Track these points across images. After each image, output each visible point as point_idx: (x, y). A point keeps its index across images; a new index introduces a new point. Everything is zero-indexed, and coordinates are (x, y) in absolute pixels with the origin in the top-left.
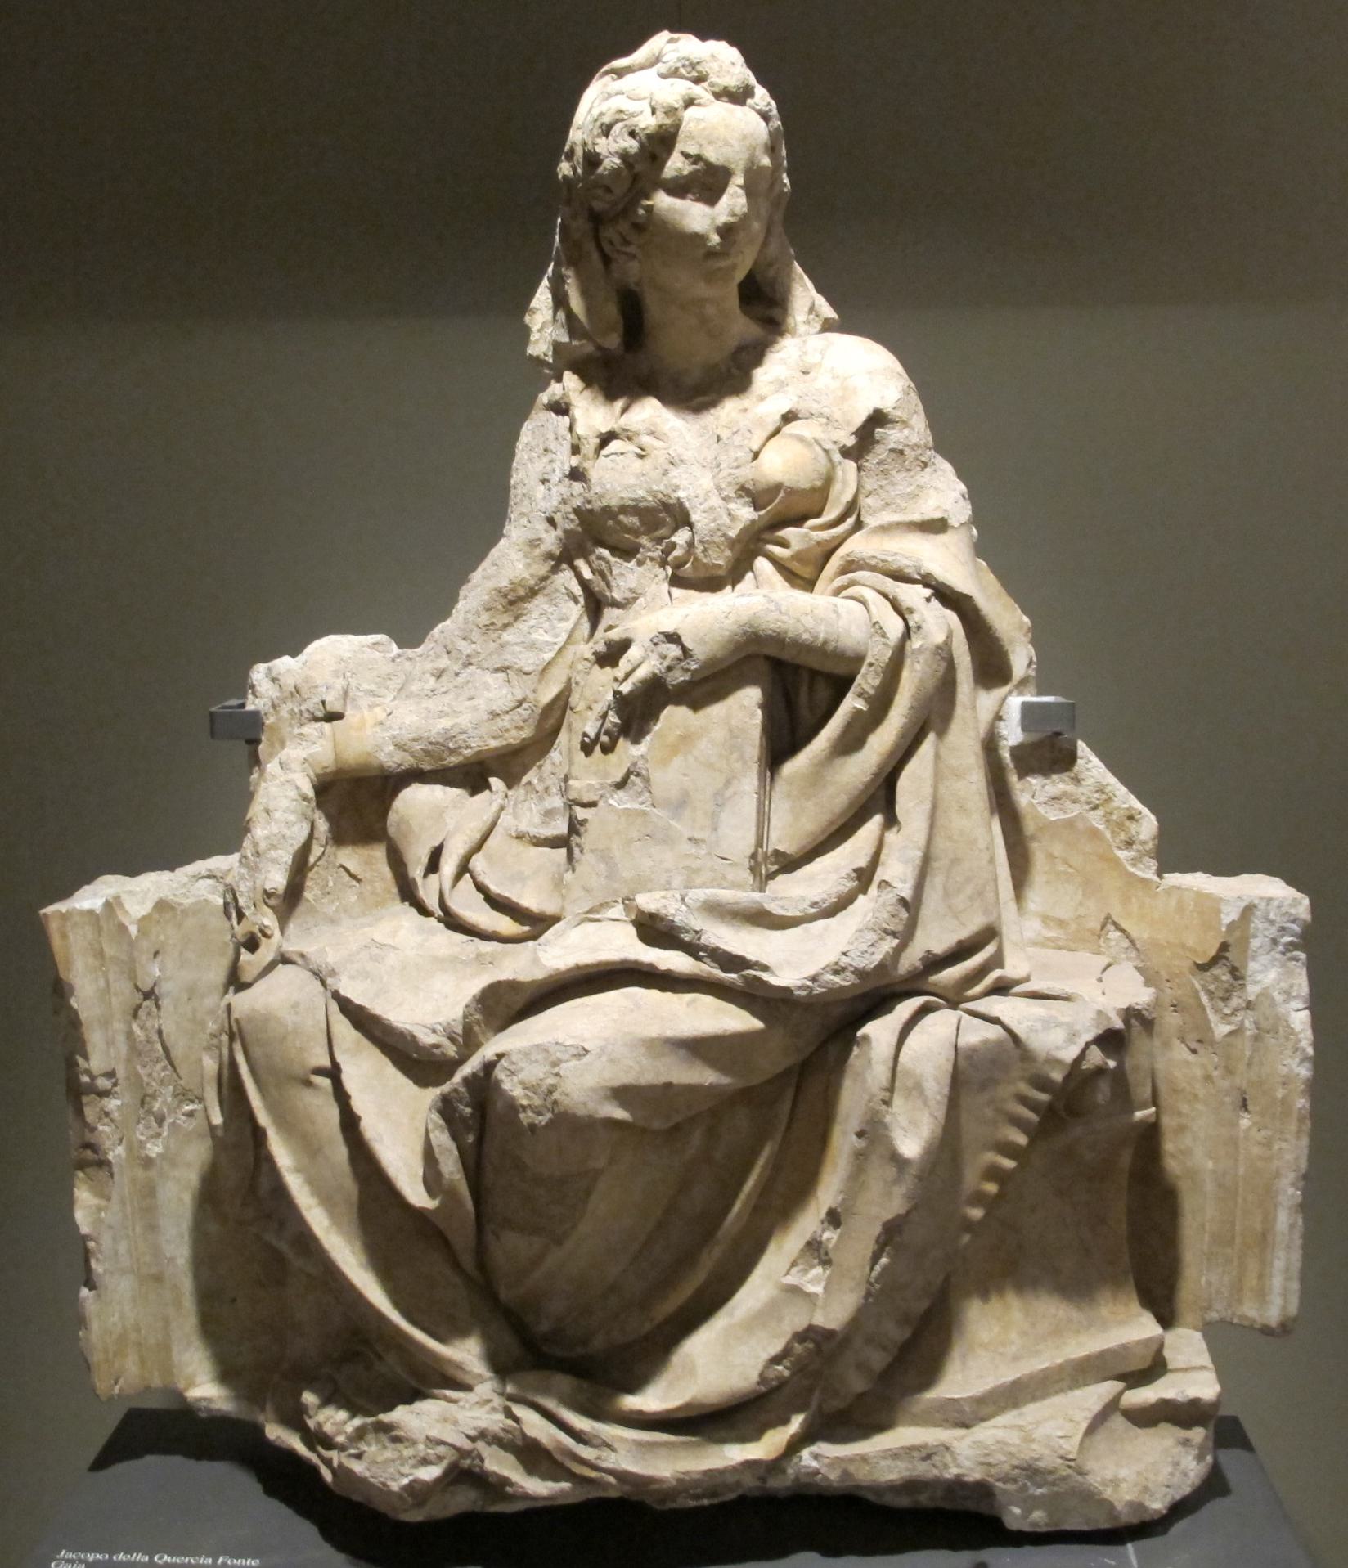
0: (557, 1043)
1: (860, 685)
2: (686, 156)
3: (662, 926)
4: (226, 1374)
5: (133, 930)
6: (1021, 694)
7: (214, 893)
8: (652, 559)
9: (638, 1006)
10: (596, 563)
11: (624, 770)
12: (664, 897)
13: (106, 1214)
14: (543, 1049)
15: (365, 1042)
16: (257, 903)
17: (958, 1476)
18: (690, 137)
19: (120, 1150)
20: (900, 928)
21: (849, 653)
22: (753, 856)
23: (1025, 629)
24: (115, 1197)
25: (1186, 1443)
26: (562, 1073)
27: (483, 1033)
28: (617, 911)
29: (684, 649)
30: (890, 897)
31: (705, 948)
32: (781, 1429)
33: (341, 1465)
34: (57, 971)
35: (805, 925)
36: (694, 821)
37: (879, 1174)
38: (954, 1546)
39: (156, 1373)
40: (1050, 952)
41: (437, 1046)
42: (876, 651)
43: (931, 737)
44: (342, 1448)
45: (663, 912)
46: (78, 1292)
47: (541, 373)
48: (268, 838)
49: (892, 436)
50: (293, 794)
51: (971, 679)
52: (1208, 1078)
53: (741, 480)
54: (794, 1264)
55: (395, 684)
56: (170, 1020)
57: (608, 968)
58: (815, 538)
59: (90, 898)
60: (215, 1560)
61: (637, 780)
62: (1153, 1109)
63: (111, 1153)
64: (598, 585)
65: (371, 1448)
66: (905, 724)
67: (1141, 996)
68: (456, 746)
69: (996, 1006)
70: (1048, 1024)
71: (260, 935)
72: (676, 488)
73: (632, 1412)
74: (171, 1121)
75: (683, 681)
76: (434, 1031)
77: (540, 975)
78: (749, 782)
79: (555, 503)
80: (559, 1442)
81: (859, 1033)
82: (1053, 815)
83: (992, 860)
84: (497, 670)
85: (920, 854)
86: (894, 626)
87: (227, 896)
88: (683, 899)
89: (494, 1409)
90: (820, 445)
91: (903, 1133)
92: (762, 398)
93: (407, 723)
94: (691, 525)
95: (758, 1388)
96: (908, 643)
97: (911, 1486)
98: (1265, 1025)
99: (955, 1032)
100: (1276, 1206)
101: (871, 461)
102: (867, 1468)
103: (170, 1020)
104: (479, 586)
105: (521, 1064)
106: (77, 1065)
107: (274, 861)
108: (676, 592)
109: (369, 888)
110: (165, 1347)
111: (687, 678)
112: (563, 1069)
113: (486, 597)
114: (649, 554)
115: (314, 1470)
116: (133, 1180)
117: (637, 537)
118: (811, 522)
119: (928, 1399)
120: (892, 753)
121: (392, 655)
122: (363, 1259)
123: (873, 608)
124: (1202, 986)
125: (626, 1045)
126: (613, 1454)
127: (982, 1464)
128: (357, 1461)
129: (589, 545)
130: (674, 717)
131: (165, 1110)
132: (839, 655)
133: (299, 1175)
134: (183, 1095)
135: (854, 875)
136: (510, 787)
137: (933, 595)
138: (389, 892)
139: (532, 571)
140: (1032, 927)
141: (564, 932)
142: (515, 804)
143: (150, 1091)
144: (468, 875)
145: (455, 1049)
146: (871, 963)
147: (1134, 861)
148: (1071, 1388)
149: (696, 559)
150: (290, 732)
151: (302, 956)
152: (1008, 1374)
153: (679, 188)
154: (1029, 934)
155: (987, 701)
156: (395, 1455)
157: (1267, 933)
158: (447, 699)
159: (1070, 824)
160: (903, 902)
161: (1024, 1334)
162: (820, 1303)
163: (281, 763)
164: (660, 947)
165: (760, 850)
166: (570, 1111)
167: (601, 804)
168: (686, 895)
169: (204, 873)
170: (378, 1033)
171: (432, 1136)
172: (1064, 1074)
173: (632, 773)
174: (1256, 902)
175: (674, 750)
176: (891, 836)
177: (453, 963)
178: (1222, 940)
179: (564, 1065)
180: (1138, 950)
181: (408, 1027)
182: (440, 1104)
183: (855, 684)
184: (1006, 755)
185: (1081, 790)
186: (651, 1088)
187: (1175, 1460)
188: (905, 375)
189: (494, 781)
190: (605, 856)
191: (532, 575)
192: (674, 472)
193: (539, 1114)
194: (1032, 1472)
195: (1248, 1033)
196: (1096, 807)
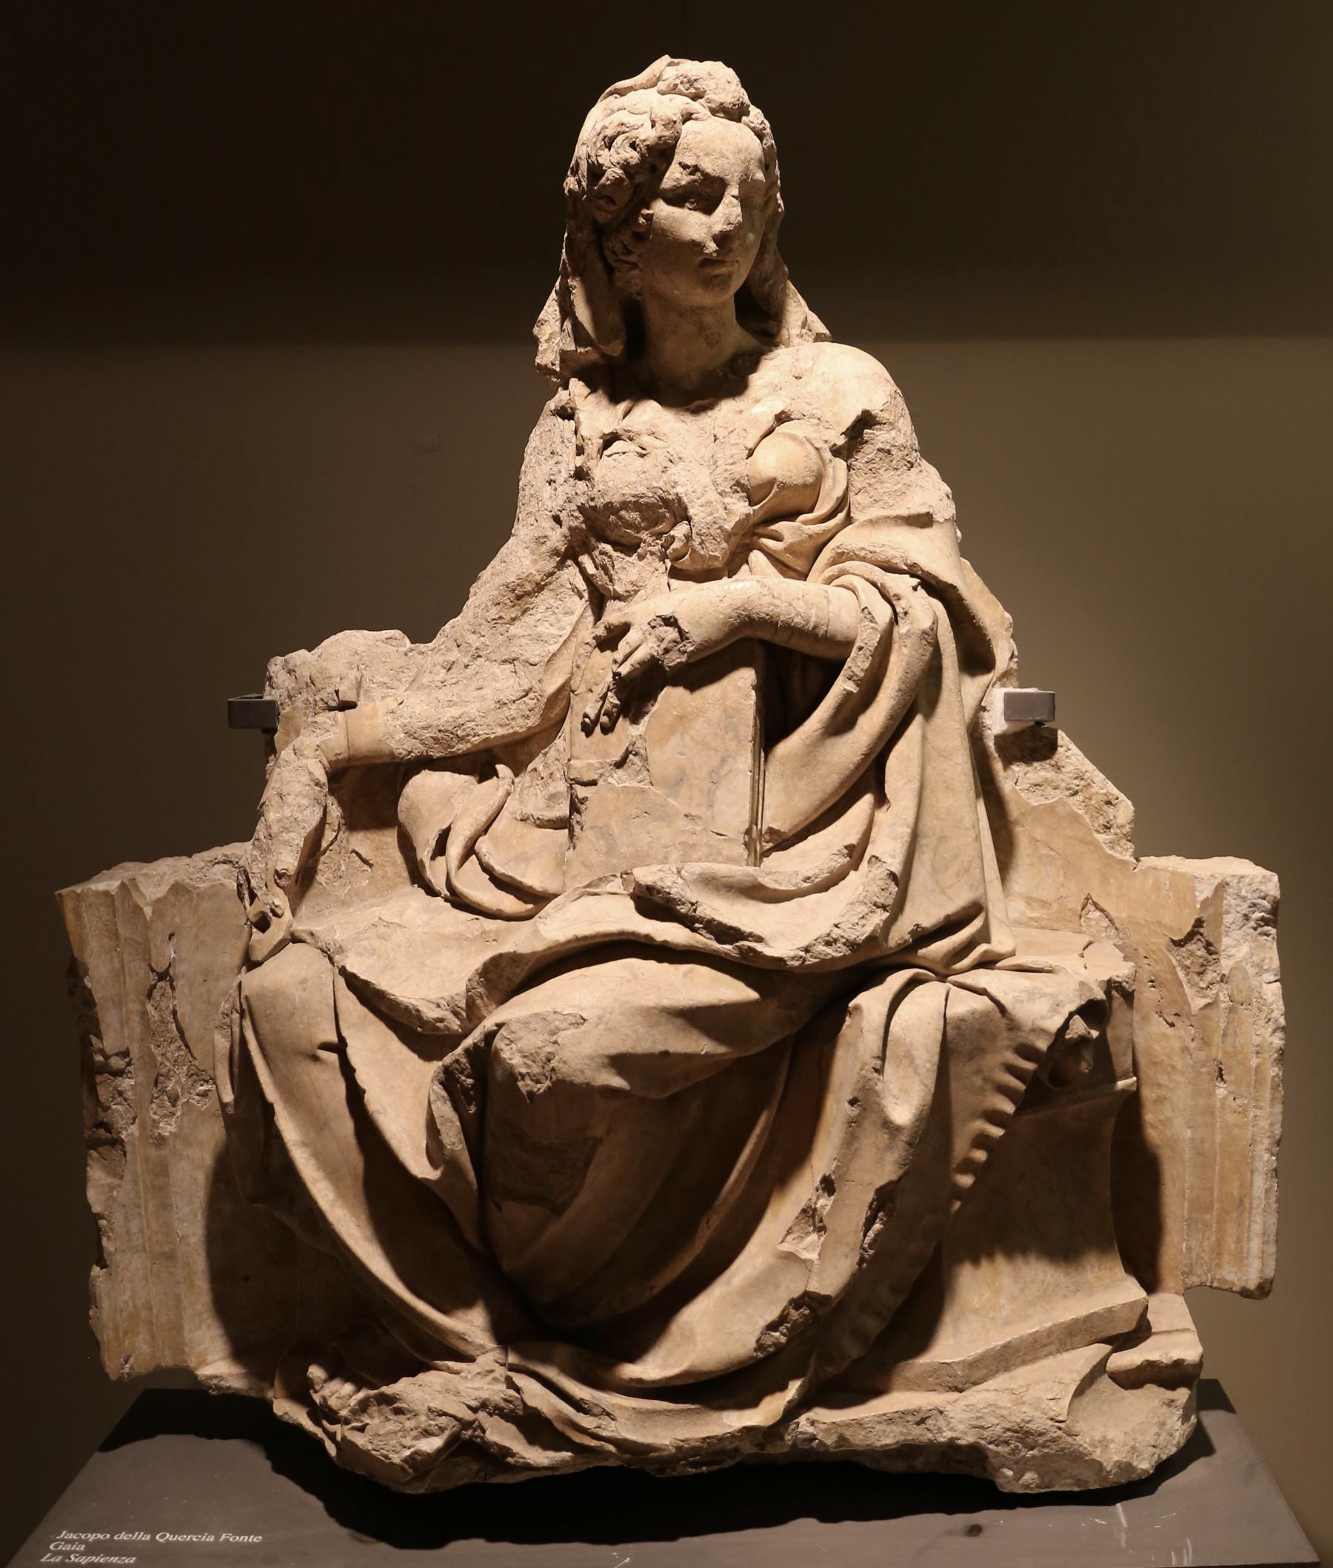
0: (555, 1012)
1: (850, 668)
2: (685, 167)
3: (657, 898)
4: (239, 1353)
5: (148, 911)
6: (1004, 685)
7: (230, 878)
8: (652, 553)
9: (636, 977)
10: (599, 559)
11: (624, 750)
12: (660, 870)
13: (118, 1192)
14: (543, 1018)
15: (371, 1016)
16: (268, 883)
17: (952, 1440)
18: (688, 149)
19: (134, 1129)
20: (890, 901)
21: (840, 638)
22: (748, 832)
23: (1007, 624)
24: (128, 1176)
25: (1170, 1403)
26: (559, 1041)
27: (486, 1006)
28: (616, 885)
29: (681, 632)
30: (880, 872)
31: (700, 920)
32: (778, 1395)
33: (344, 1438)
34: (71, 949)
35: (798, 899)
36: (691, 798)
37: (872, 1140)
38: (950, 1510)
39: (167, 1352)
40: (1034, 932)
41: (441, 1020)
42: (865, 635)
43: (919, 719)
44: (347, 1422)
45: (660, 884)
46: (90, 1270)
47: (548, 382)
48: (279, 821)
49: (878, 437)
50: (306, 779)
51: (956, 665)
52: (1185, 1049)
53: (737, 476)
54: (789, 1232)
55: (406, 677)
56: (184, 1001)
57: (607, 939)
58: (807, 532)
59: (106, 883)
60: (218, 1537)
61: (636, 760)
62: (1135, 1079)
63: (124, 1132)
64: (601, 579)
65: (374, 1420)
66: (893, 706)
67: (1121, 970)
68: (464, 733)
69: (981, 978)
70: (1032, 995)
71: (270, 914)
72: (675, 484)
73: (631, 1380)
74: (184, 1100)
75: (679, 663)
76: (438, 1006)
77: (539, 946)
78: (744, 761)
79: (561, 502)
80: (559, 1411)
81: (851, 1005)
82: (1035, 800)
83: (978, 838)
84: (504, 662)
85: (909, 830)
86: (883, 613)
87: (240, 877)
88: (679, 872)
89: (495, 1379)
90: (812, 444)
91: (894, 1100)
92: (757, 401)
93: (418, 712)
94: (689, 519)
95: (755, 1354)
96: (896, 629)
97: (907, 1450)
98: (1239, 998)
99: (944, 1002)
100: (1252, 1172)
101: (860, 459)
102: (863, 1433)
103: (184, 1001)
104: (489, 582)
105: (522, 1033)
106: (91, 1044)
107: (286, 843)
108: (675, 583)
109: (380, 872)
110: (177, 1327)
111: (684, 660)
112: (561, 1037)
113: (495, 592)
114: (650, 548)
115: (320, 1443)
116: (146, 1159)
117: (638, 532)
118: (803, 517)
119: (921, 1364)
120: (881, 736)
121: (405, 649)
122: (368, 1231)
123: (861, 594)
124: (1179, 961)
125: (622, 1014)
126: (613, 1422)
127: (975, 1427)
128: (360, 1433)
129: (593, 540)
130: (672, 697)
131: (179, 1090)
132: (829, 640)
133: (305, 1149)
134: (197, 1075)
135: (846, 851)
136: (516, 775)
137: (919, 584)
138: (400, 876)
139: (538, 567)
140: (1017, 908)
141: (564, 905)
142: (522, 790)
143: (164, 1071)
144: (474, 856)
145: (458, 1023)
146: (863, 935)
147: (1112, 844)
148: (1058, 1352)
149: (694, 551)
150: (304, 721)
151: (312, 934)
152: (998, 1340)
153: (677, 198)
154: (1014, 915)
155: (973, 687)
156: (398, 1426)
157: (1238, 909)
158: (456, 689)
159: (1051, 809)
160: (892, 876)
161: (1013, 1299)
162: (815, 1268)
163: (294, 750)
164: (657, 919)
165: (754, 826)
166: (568, 1079)
167: (600, 782)
168: (683, 868)
169: (221, 858)
170: (384, 1009)
171: (433, 1106)
172: (1049, 1044)
173: (631, 752)
174: (1228, 880)
175: (672, 730)
176: (881, 815)
177: (459, 940)
178: (1197, 917)
179: (562, 1034)
180: (1117, 929)
181: (413, 1001)
182: (442, 1075)
183: (845, 667)
184: (991, 744)
185: (1061, 776)
186: (649, 1057)
187: (1162, 1420)
188: (892, 382)
189: (501, 768)
190: (604, 833)
191: (538, 571)
192: (673, 469)
193: (538, 1082)
194: (1024, 1435)
195: (1223, 1005)
196: (1076, 793)
